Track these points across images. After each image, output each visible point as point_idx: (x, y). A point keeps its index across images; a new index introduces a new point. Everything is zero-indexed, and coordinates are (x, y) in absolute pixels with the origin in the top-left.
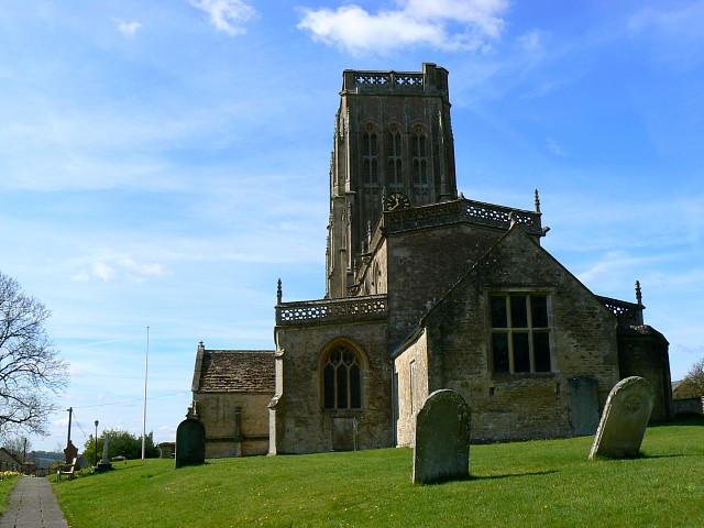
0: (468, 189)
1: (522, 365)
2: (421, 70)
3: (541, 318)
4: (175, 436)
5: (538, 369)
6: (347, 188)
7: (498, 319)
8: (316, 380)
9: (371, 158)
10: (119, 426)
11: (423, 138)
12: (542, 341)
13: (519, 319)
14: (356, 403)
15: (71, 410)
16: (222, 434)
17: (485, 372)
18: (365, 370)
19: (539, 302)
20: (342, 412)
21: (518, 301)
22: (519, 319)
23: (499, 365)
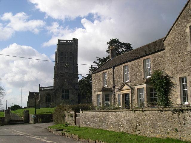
0: (52, 84)
1: (66, 98)
2: (72, 39)
3: (68, 92)
4: (136, 48)
5: (68, 98)
6: (57, 62)
7: (63, 92)
8: (44, 98)
9: (62, 57)
10: (15, 104)
11: (72, 53)
12: (68, 95)
13: (66, 92)
14: (50, 101)
15: (7, 100)
16: (33, 105)
17: (61, 99)
18: (51, 97)
19: (68, 90)
20: (48, 103)
21: (66, 90)
22: (66, 92)
23: (63, 97)
